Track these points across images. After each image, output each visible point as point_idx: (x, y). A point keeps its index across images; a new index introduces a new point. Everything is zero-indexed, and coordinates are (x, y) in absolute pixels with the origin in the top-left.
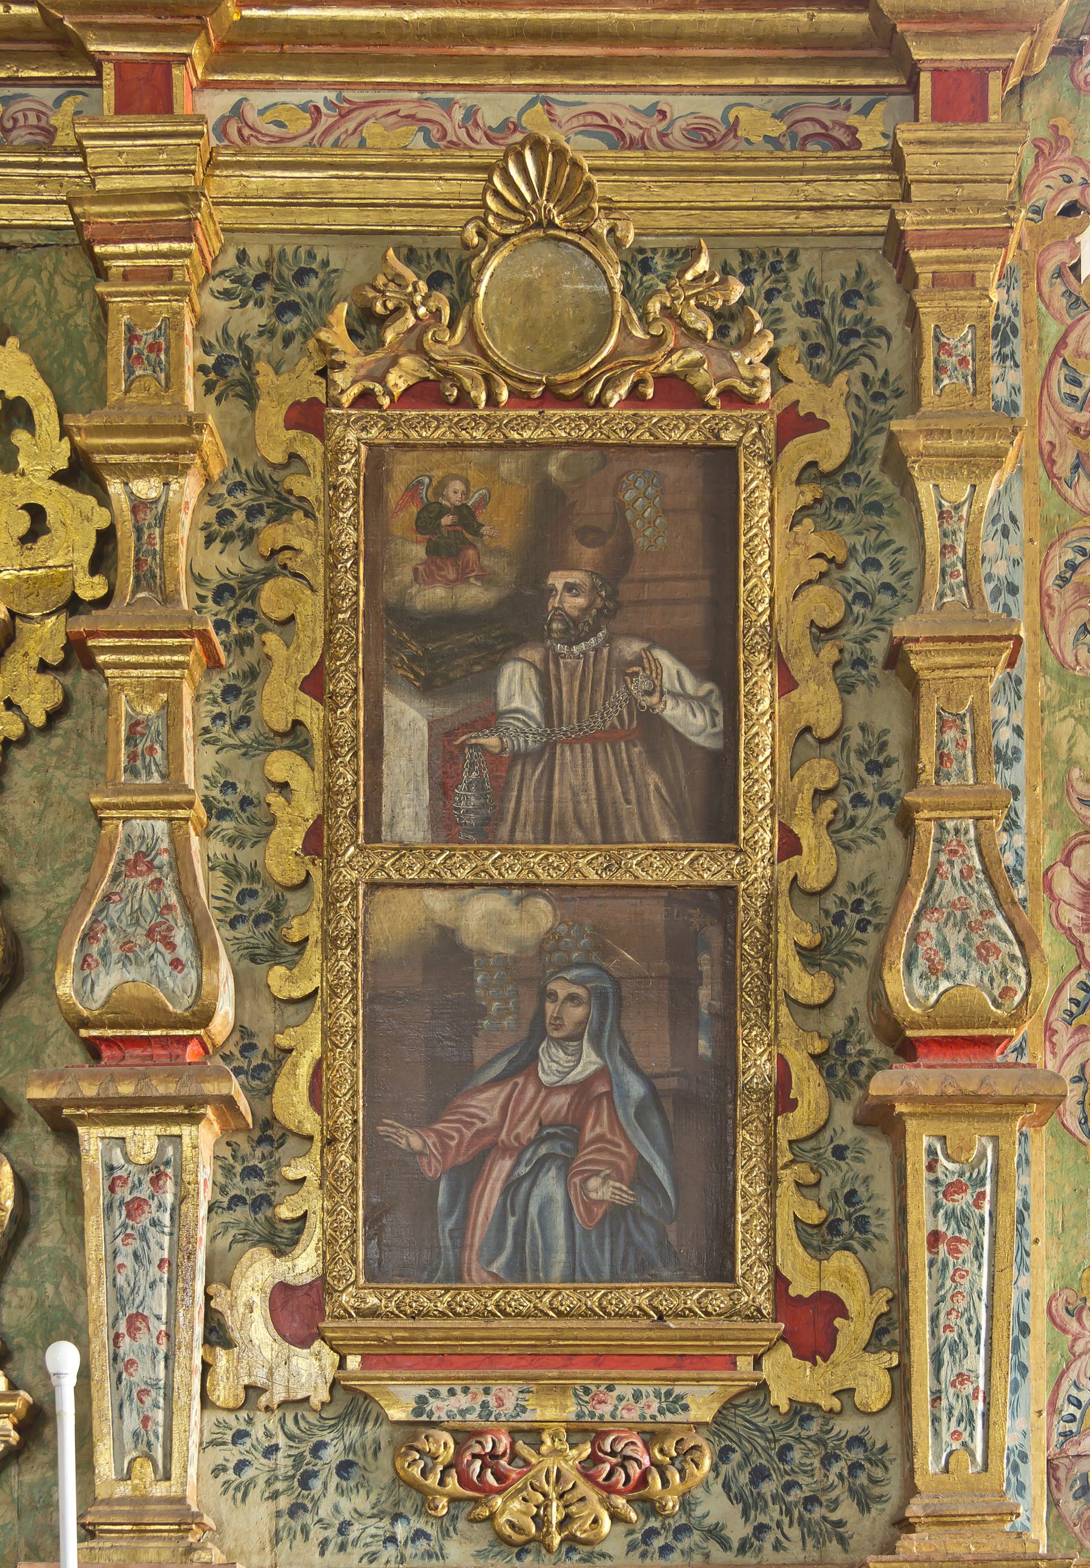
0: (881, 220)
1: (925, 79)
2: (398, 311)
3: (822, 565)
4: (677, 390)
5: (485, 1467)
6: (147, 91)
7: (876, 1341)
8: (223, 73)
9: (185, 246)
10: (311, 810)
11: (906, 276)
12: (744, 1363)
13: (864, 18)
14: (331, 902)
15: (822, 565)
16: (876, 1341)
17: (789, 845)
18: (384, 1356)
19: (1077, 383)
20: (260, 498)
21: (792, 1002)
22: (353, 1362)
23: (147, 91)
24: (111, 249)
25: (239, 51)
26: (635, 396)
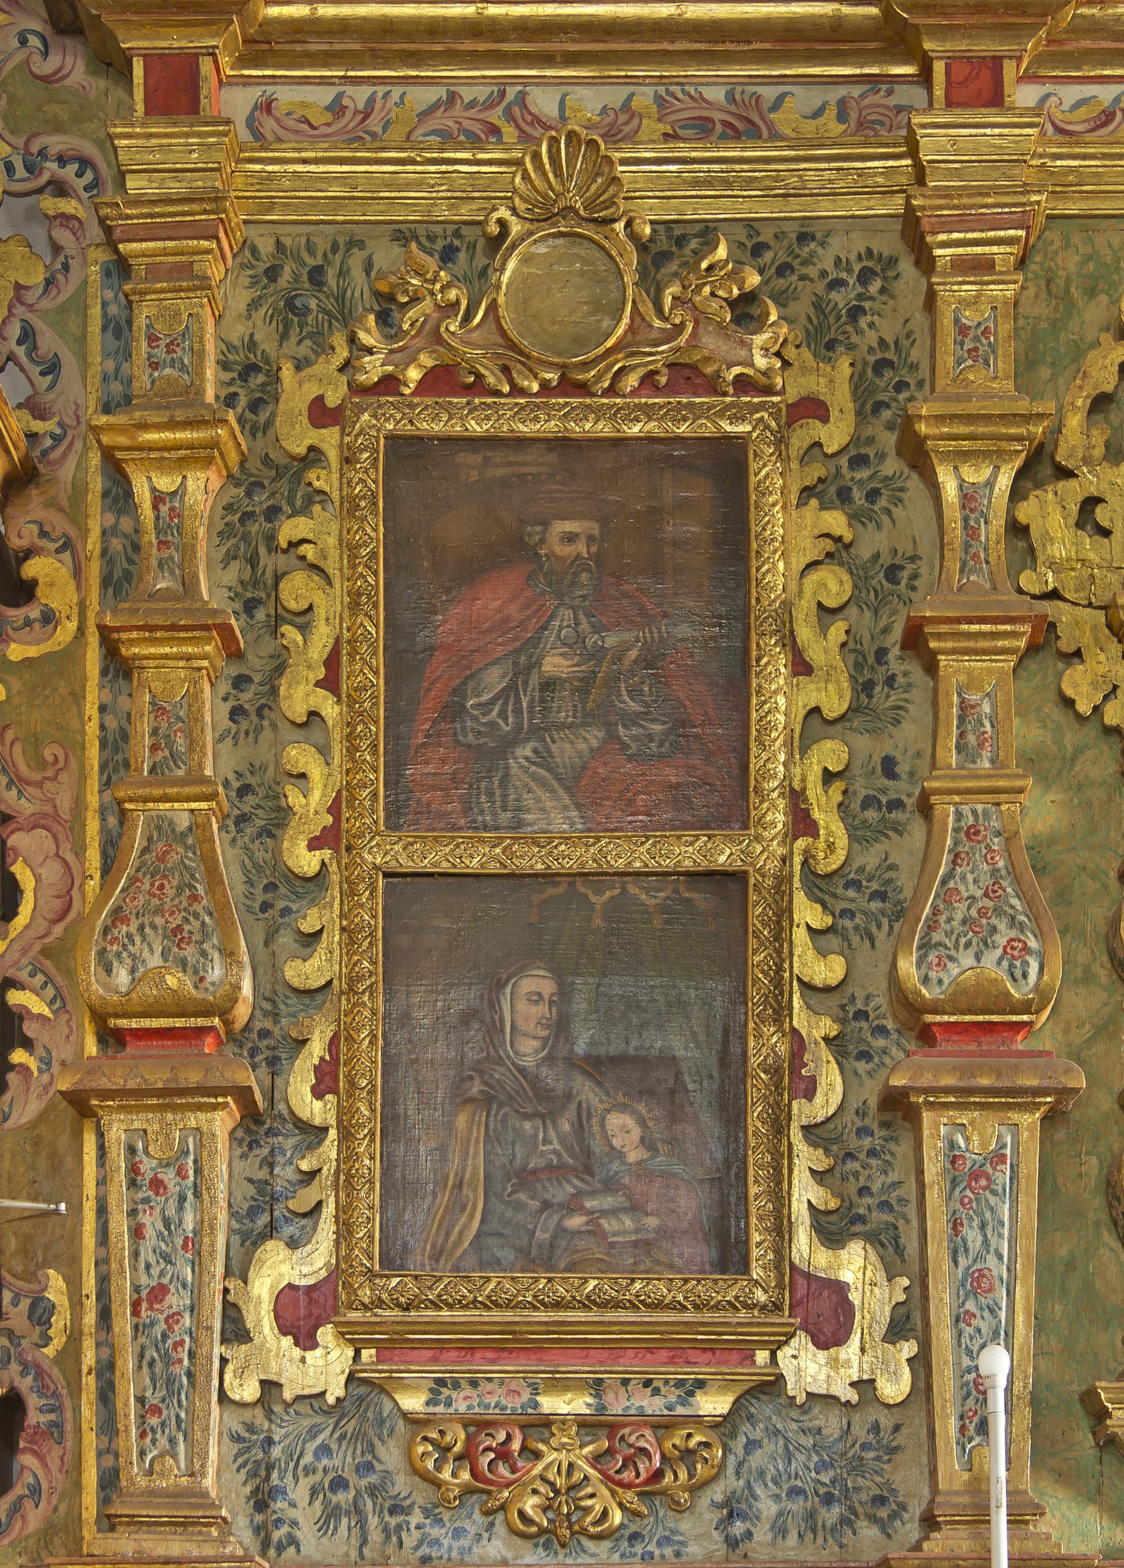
0: (897, 204)
1: (939, 67)
2: (415, 300)
3: (829, 545)
4: (687, 375)
5: (494, 1452)
6: (177, 92)
7: (896, 1331)
8: (256, 67)
9: (205, 244)
10: (636, 1132)
11: (925, 261)
12: (762, 1357)
13: (873, 11)
14: (350, 891)
15: (829, 545)
16: (896, 1331)
17: (802, 822)
18: (393, 1346)
19: (40, 414)
20: (270, 486)
21: (807, 987)
22: (367, 1354)
23: (177, 92)
24: (135, 246)
25: (267, 46)
26: (649, 379)
